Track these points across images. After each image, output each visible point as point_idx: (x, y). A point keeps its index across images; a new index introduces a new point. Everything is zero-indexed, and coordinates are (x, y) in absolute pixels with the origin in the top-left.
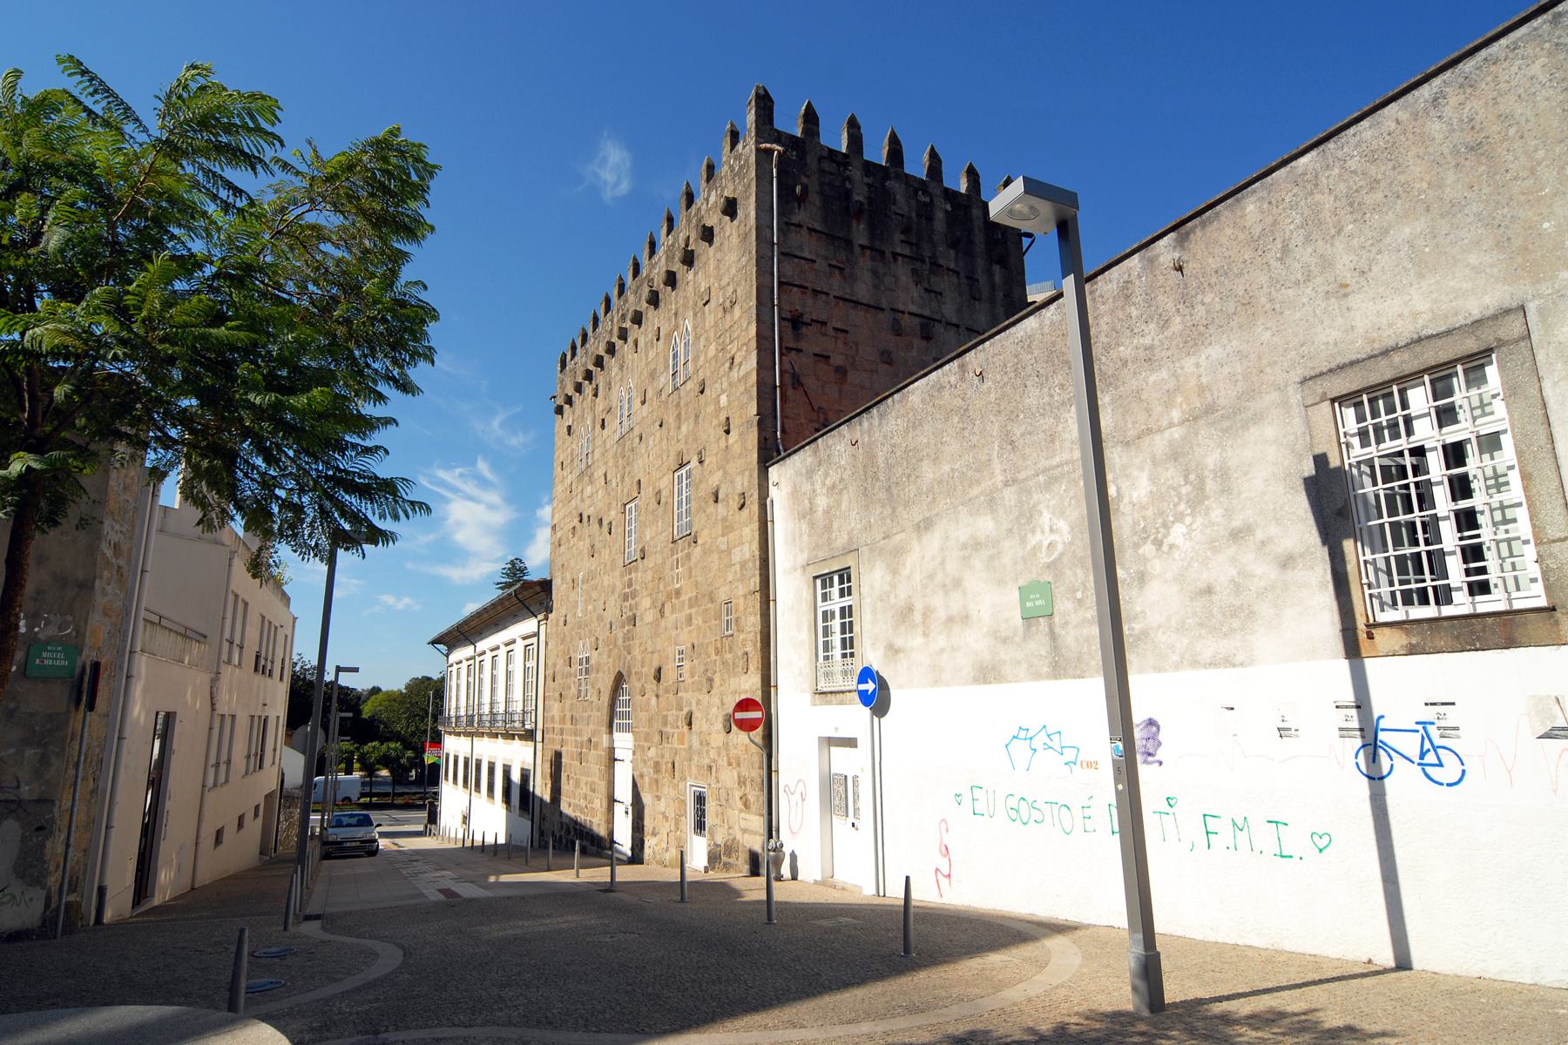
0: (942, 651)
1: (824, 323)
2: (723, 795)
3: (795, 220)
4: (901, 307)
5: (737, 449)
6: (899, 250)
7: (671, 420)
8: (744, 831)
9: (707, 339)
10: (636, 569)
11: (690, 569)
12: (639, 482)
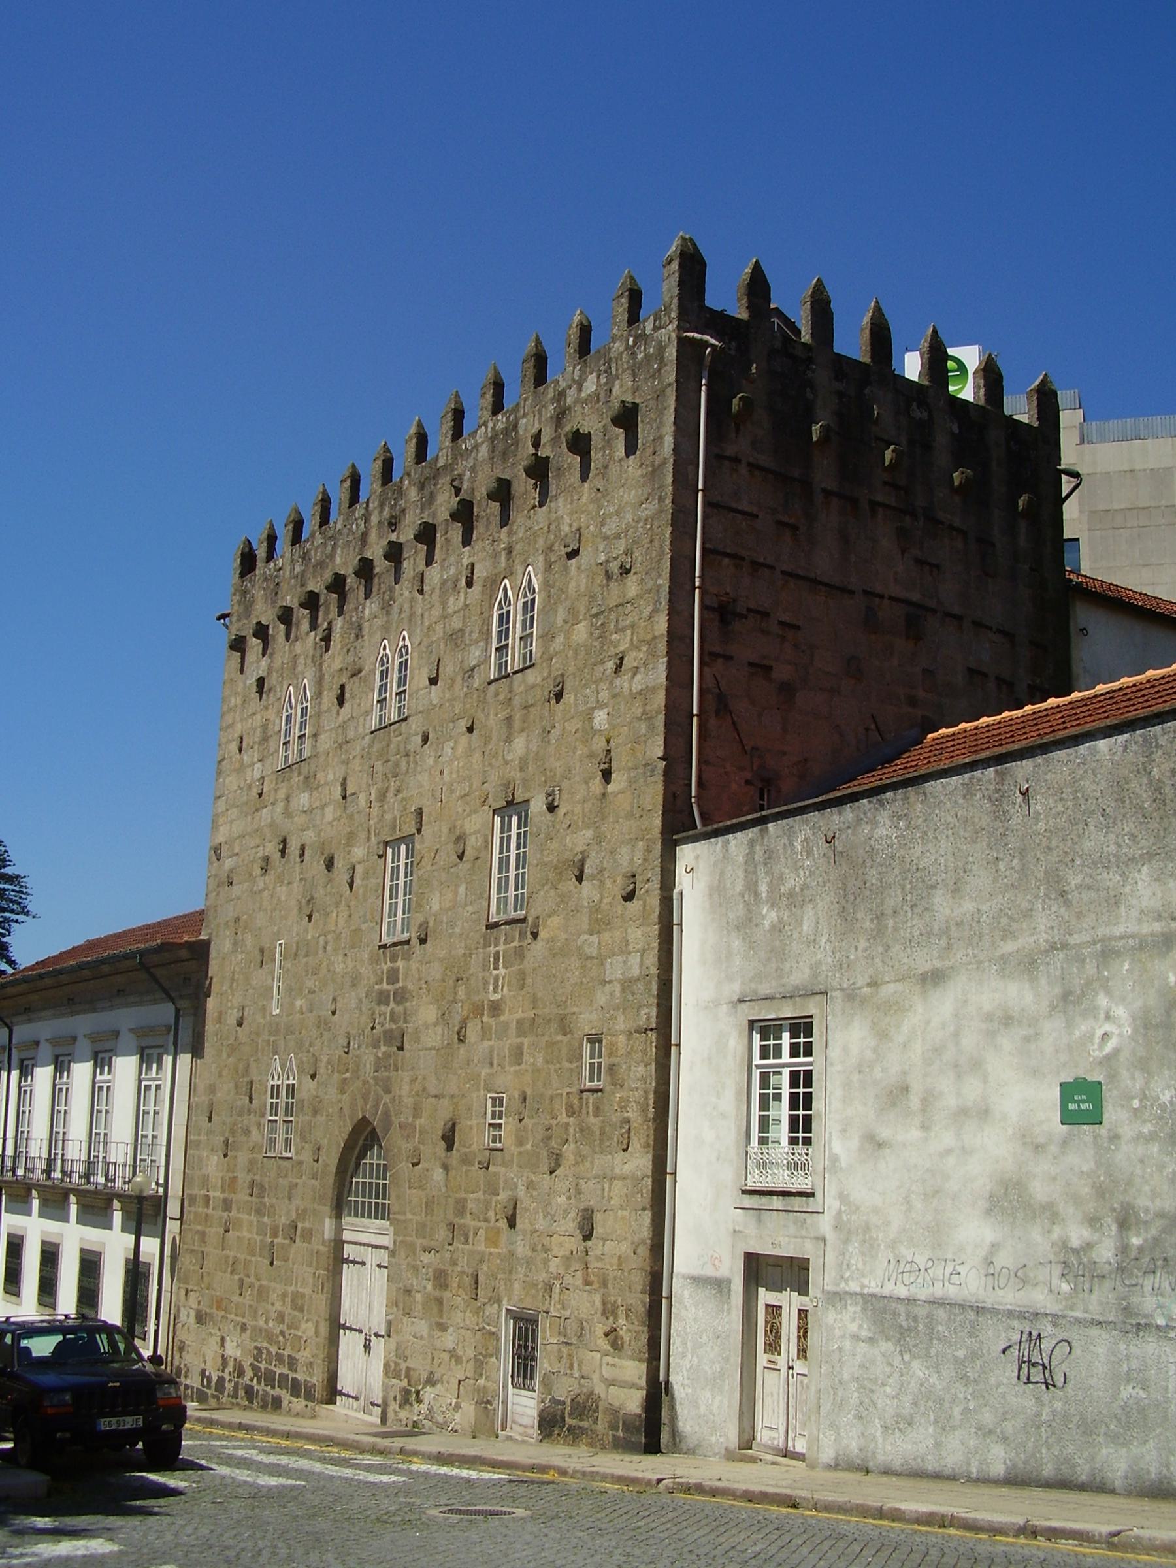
0: (949, 1151)
1: (765, 615)
2: (572, 1326)
3: (730, 450)
4: (879, 589)
5: (624, 803)
6: (879, 498)
7: (492, 720)
8: (611, 1383)
9: (572, 611)
10: (407, 958)
11: (522, 976)
12: (420, 812)
